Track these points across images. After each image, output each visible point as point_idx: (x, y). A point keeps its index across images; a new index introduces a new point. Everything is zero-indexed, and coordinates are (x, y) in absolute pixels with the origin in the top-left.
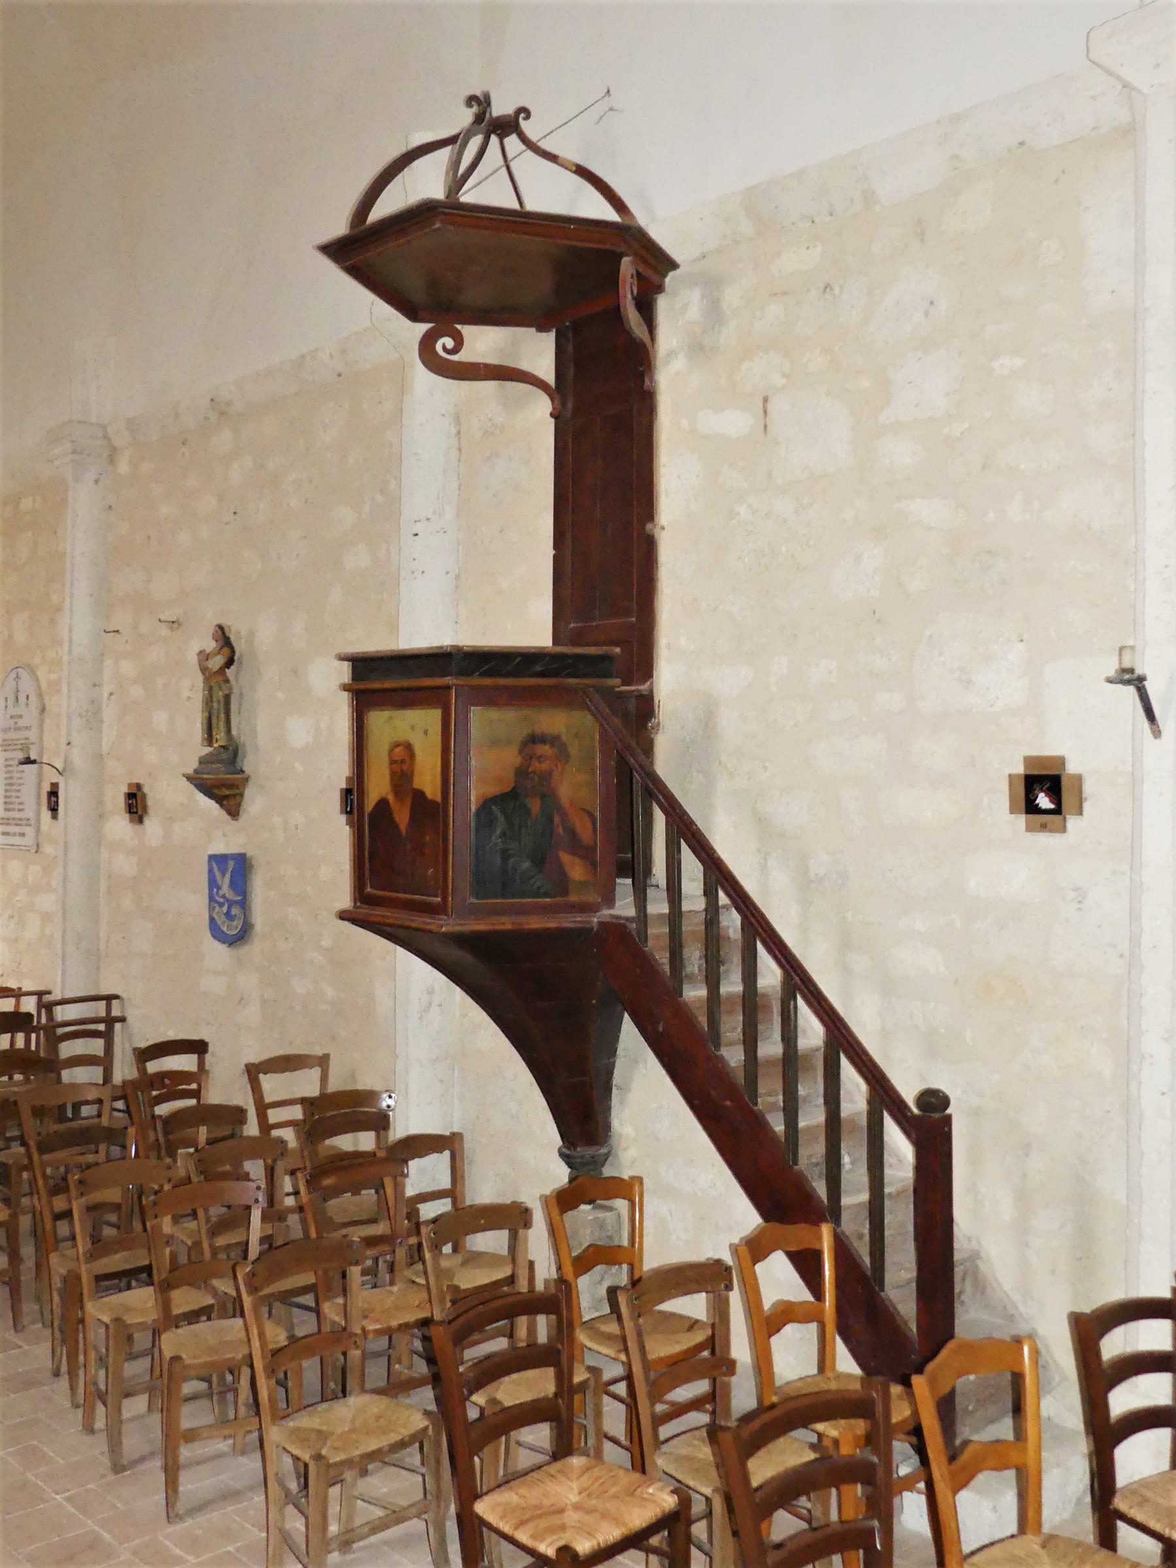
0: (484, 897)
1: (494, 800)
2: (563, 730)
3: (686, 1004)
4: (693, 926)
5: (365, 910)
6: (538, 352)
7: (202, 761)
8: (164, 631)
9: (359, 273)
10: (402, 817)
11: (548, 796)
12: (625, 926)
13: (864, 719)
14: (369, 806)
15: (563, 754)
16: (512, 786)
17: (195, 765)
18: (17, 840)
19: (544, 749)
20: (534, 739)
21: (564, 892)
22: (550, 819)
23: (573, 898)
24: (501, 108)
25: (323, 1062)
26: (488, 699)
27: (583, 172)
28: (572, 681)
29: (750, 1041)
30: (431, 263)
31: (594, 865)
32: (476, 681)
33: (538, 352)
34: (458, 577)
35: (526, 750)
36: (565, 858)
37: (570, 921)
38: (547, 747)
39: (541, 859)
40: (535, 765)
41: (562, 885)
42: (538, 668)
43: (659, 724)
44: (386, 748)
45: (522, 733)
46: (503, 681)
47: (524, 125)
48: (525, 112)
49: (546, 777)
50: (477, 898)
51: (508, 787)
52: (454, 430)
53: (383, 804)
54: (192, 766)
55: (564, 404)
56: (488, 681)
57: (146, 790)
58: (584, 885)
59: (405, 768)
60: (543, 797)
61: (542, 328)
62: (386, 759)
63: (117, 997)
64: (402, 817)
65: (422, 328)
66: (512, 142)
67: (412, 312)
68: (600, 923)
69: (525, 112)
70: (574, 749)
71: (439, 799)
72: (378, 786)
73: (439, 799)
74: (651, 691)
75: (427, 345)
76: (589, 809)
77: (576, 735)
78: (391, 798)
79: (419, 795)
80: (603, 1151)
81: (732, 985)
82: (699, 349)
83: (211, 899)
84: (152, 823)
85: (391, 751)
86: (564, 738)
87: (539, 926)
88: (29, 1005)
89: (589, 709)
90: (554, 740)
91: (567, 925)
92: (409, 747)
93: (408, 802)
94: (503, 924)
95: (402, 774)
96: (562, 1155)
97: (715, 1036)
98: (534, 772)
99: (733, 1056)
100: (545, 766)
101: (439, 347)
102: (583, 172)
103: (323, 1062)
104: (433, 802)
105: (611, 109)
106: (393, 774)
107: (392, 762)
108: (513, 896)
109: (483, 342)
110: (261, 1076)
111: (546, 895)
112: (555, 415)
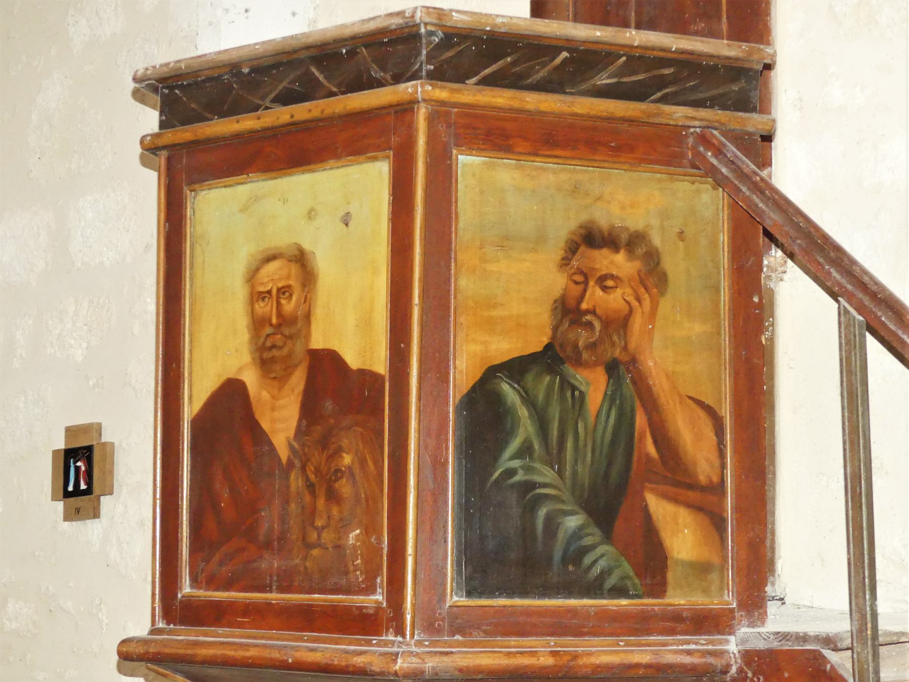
0: (481, 594)
1: (516, 368)
2: (655, 222)
5: (184, 637)
10: (280, 418)
11: (623, 371)
12: (817, 657)
13: (315, 552)
14: (195, 399)
15: (653, 275)
16: (545, 340)
19: (618, 263)
20: (591, 238)
21: (658, 588)
22: (625, 422)
23: (678, 598)
26: (496, 136)
28: (678, 113)
31: (718, 523)
32: (470, 94)
35: (575, 263)
36: (659, 507)
37: (677, 650)
38: (620, 258)
39: (609, 502)
40: (595, 296)
41: (652, 565)
42: (604, 80)
44: (239, 268)
45: (563, 225)
46: (534, 101)
49: (619, 324)
50: (469, 594)
51: (536, 343)
53: (231, 393)
56: (501, 98)
58: (702, 569)
59: (289, 307)
60: (612, 368)
62: (240, 293)
64: (280, 418)
68: (749, 656)
70: (674, 264)
71: (380, 364)
72: (221, 352)
73: (380, 364)
76: (709, 401)
77: (681, 235)
78: (251, 378)
79: (326, 366)
85: (252, 276)
86: (657, 240)
87: (606, 659)
89: (712, 172)
90: (633, 242)
91: (670, 658)
92: (301, 259)
93: (298, 380)
94: (533, 654)
95: (279, 327)
98: (593, 312)
100: (614, 300)
104: (368, 377)
106: (258, 324)
107: (256, 296)
108: (547, 591)
111: (619, 591)
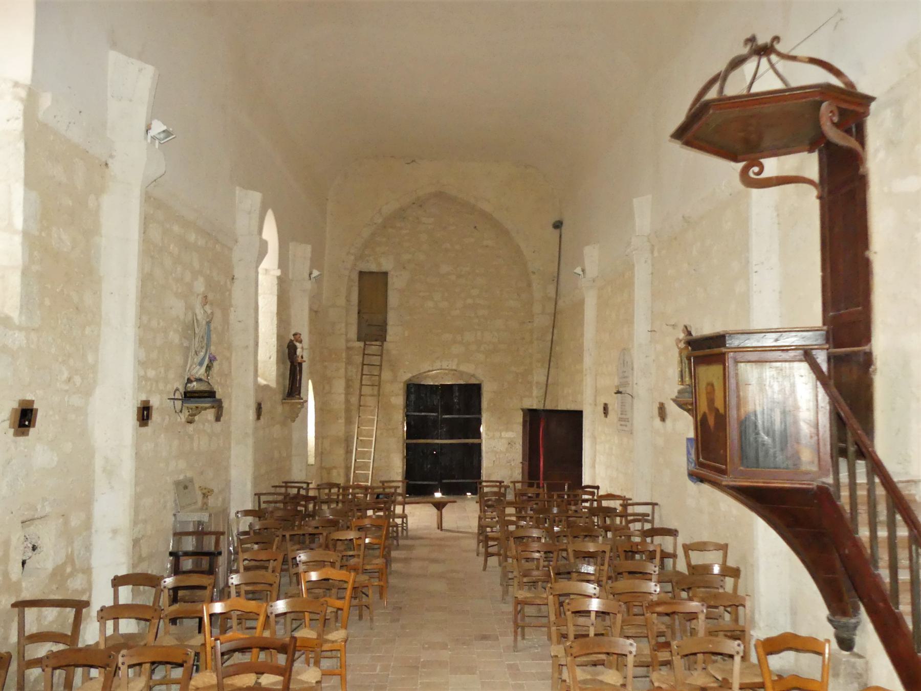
3: (860, 539)
4: (862, 493)
5: (703, 472)
6: (809, 164)
7: (680, 392)
8: (670, 329)
9: (689, 143)
17: (676, 394)
18: (624, 428)
24: (763, 39)
25: (724, 548)
27: (813, 61)
29: (894, 569)
30: (729, 129)
33: (809, 164)
34: (780, 292)
43: (876, 369)
47: (779, 47)
48: (776, 39)
52: (775, 214)
54: (675, 394)
55: (823, 191)
57: (666, 406)
61: (811, 151)
63: (657, 504)
65: (741, 165)
66: (774, 58)
67: (735, 158)
69: (776, 39)
74: (871, 349)
75: (744, 172)
80: (853, 621)
81: (883, 533)
82: (892, 144)
83: (688, 460)
84: (669, 421)
88: (616, 504)
96: (830, 621)
97: (874, 560)
99: (884, 574)
101: (751, 175)
102: (813, 61)
103: (724, 548)
105: (841, 20)
109: (772, 166)
110: (690, 552)
112: (820, 197)
